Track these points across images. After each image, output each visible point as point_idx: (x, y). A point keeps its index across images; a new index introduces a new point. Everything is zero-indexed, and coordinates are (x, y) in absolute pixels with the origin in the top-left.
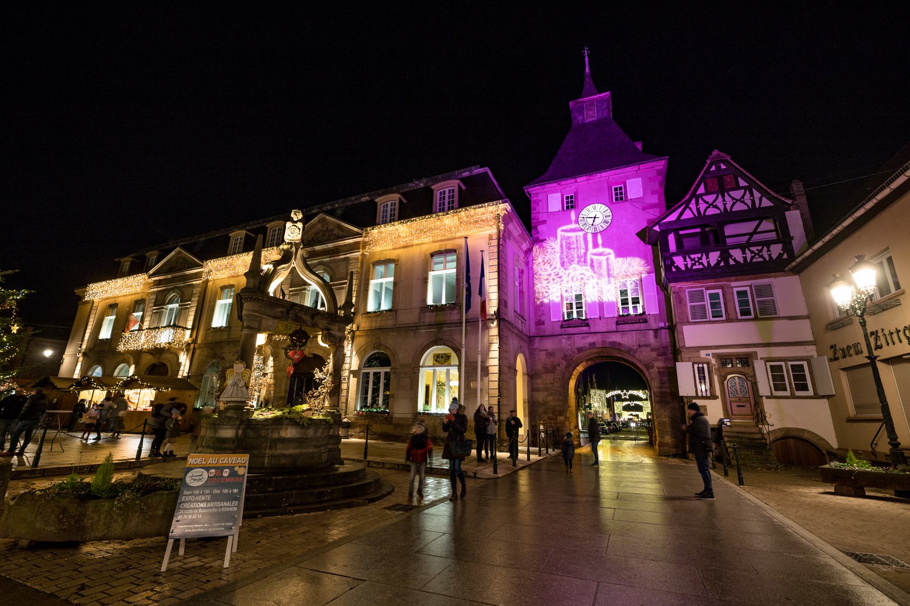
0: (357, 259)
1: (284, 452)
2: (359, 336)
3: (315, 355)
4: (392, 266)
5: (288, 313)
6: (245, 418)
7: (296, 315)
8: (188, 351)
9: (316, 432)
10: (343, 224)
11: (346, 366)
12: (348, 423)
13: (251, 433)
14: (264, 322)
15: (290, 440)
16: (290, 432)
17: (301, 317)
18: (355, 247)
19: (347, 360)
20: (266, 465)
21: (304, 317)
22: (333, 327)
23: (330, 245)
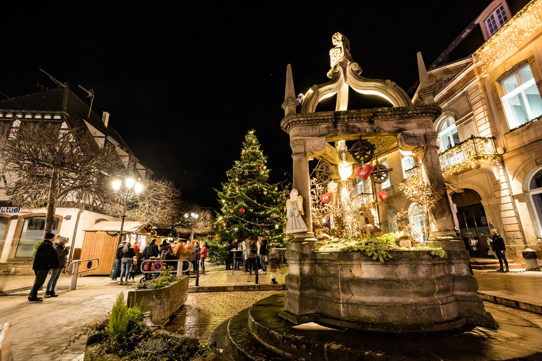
0: (477, 87)
1: (364, 299)
2: (509, 158)
3: (466, 190)
4: (527, 69)
5: (335, 127)
6: (307, 251)
7: (347, 127)
8: (375, 207)
9: (414, 270)
10: (448, 66)
11: (505, 193)
12: (534, 253)
13: (320, 271)
14: (307, 143)
15: (369, 283)
16: (366, 271)
17: (354, 127)
18: (471, 76)
19: (504, 186)
20: (343, 315)
21: (358, 125)
22: (408, 125)
23: (444, 92)
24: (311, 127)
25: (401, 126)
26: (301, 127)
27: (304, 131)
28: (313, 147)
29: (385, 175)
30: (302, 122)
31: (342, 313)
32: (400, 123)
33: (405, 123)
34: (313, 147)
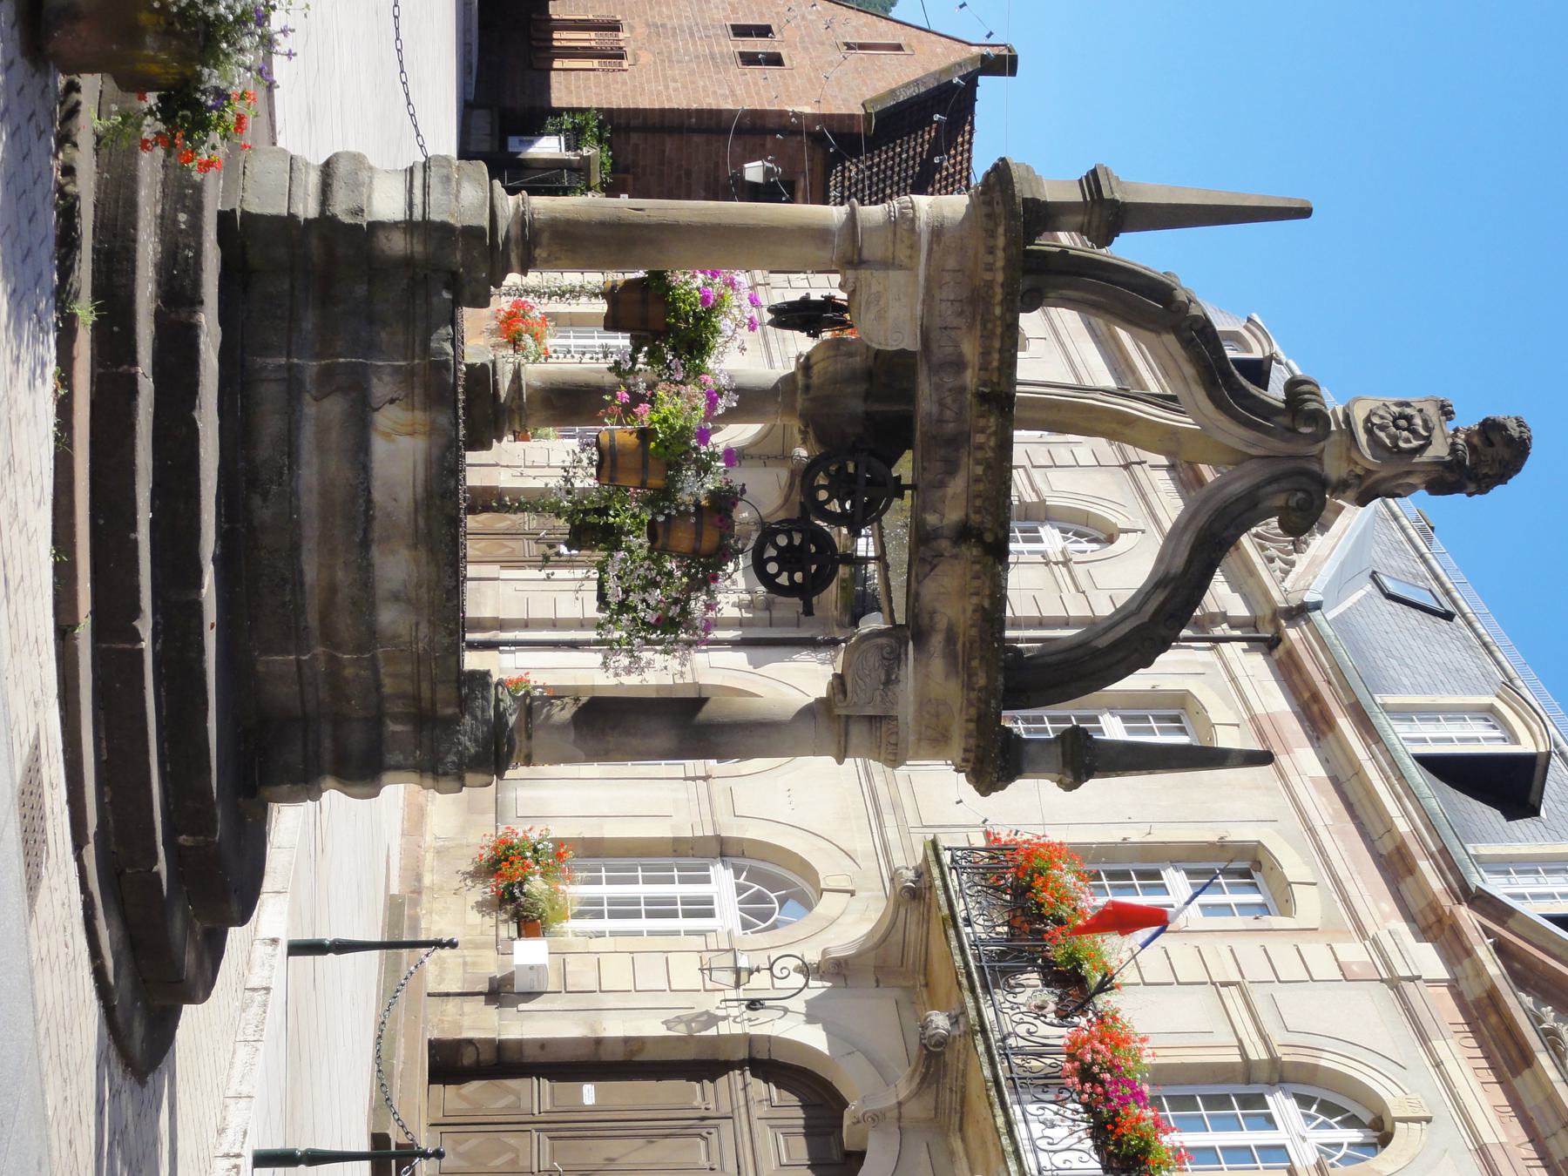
22: (937, 665)
25: (937, 642)
27: (952, 263)
28: (879, 295)
32: (951, 639)
33: (951, 656)
34: (879, 295)
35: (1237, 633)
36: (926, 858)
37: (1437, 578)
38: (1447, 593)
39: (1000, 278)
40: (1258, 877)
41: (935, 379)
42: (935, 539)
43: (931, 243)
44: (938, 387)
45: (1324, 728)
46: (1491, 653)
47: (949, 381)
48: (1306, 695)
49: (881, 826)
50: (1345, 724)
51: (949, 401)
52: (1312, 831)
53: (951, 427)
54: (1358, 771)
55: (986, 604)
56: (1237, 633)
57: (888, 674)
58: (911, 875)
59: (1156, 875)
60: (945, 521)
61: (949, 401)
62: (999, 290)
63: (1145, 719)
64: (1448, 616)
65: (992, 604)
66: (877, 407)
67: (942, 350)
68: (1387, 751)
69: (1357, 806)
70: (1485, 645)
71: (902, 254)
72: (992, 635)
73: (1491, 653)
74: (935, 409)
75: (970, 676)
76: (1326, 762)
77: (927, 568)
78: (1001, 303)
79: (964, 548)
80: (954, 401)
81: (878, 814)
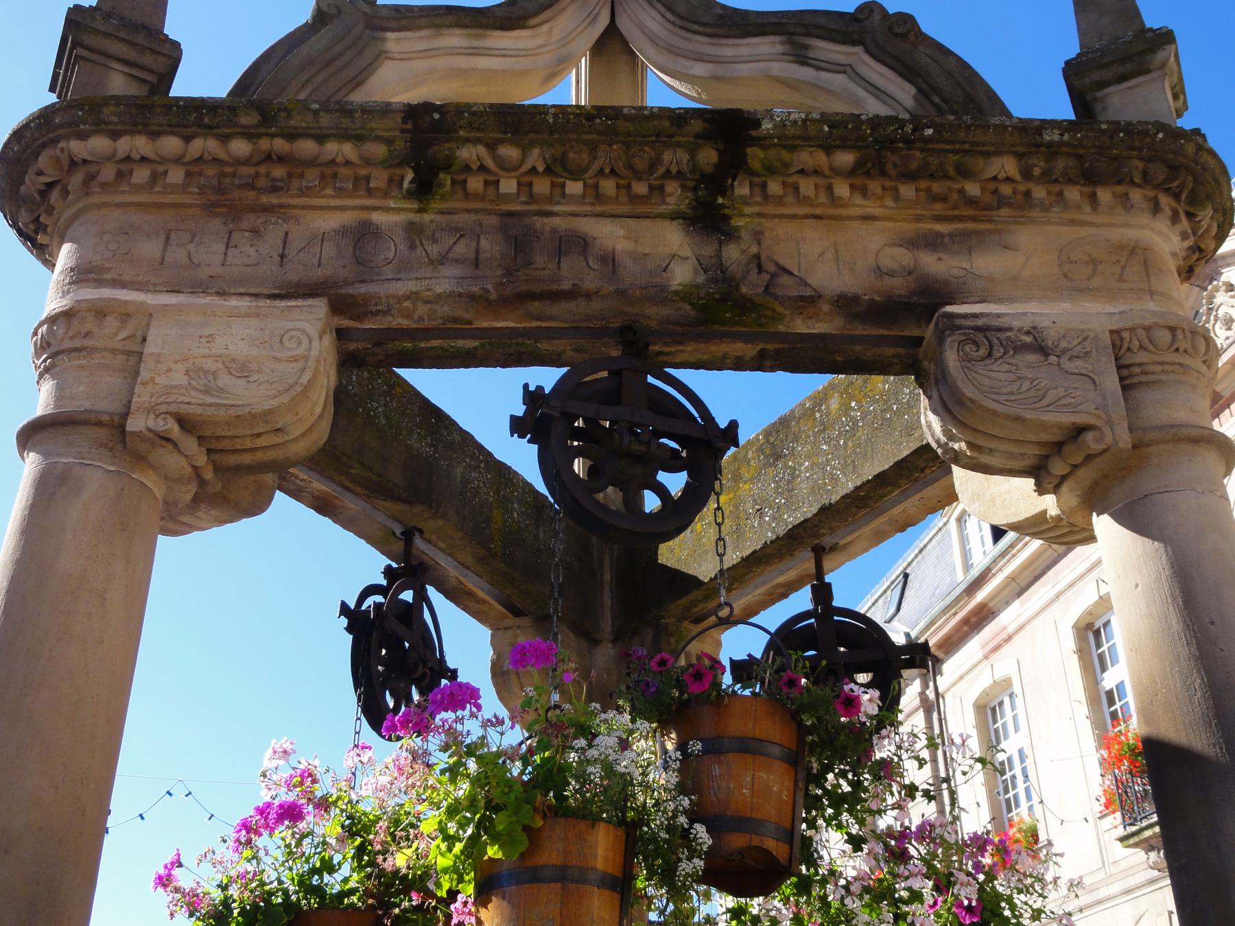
22: (987, 263)
24: (217, 224)
25: (936, 265)
26: (136, 217)
27: (150, 248)
28: (194, 372)
29: (675, 482)
30: (141, 175)
31: (599, 859)
32: (933, 243)
33: (965, 242)
34: (194, 372)
35: (931, 684)
36: (1136, 845)
37: (885, 592)
38: (893, 582)
39: (171, 144)
40: (1099, 624)
41: (388, 272)
42: (722, 268)
43: (100, 283)
44: (404, 267)
45: (985, 611)
46: (925, 546)
47: (393, 249)
48: (966, 628)
49: (1109, 899)
50: (981, 596)
51: (434, 250)
52: (1058, 596)
53: (490, 246)
54: (1012, 579)
55: (846, 159)
56: (931, 684)
57: (1021, 348)
58: (1153, 855)
59: (1110, 694)
60: (686, 251)
61: (434, 250)
62: (198, 146)
63: (996, 731)
64: (906, 576)
65: (844, 146)
66: (607, 625)
67: (330, 262)
68: (995, 562)
69: (1036, 574)
70: (921, 551)
71: (111, 333)
72: (909, 142)
73: (925, 546)
74: (450, 271)
75: (1002, 202)
76: (1008, 603)
77: (784, 280)
78: (224, 139)
79: (737, 222)
80: (434, 240)
81: (1099, 902)
